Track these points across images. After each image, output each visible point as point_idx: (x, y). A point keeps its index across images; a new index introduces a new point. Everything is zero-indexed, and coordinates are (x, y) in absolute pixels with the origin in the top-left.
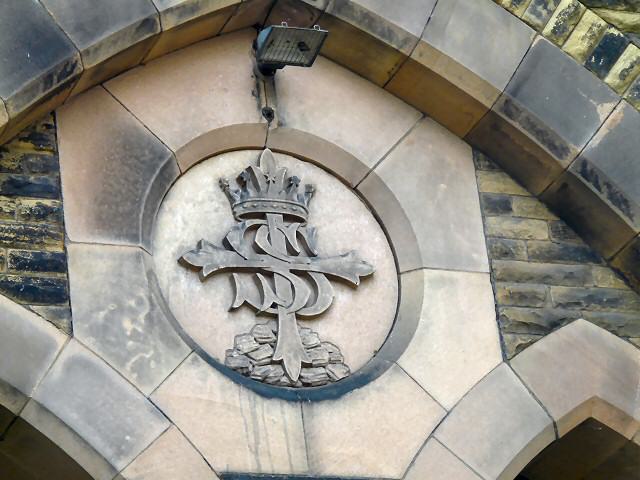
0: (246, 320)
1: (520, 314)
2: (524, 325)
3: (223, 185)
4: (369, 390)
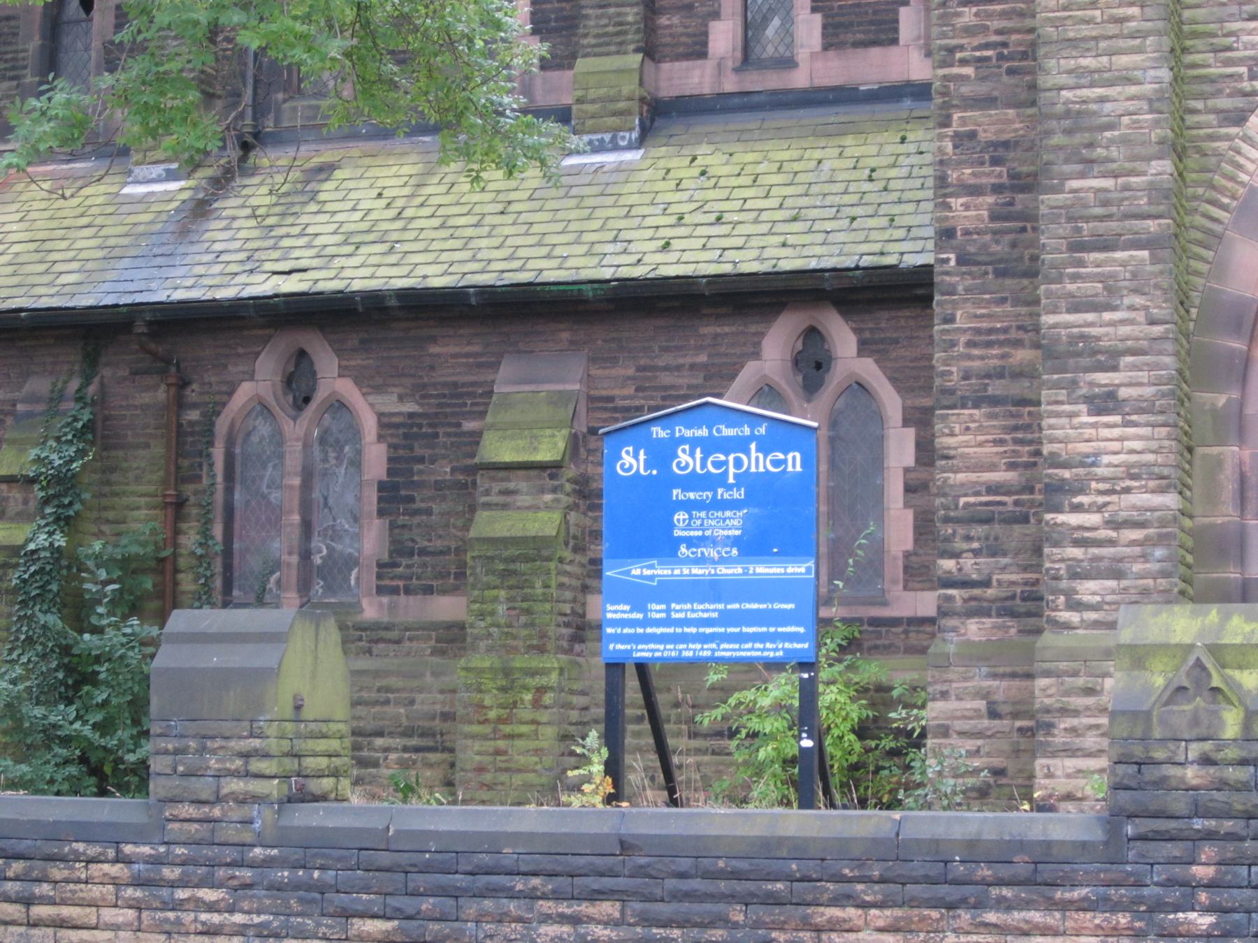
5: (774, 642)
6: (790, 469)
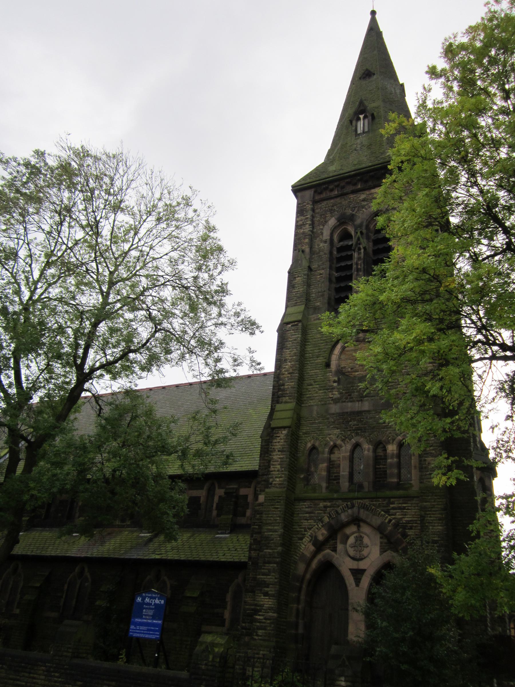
2: (383, 551)
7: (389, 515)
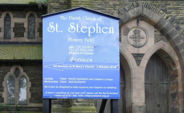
0: (134, 42)
1: (156, 40)
2: (157, 41)
3: (133, 31)
4: (143, 47)
5: (106, 92)
6: (110, 32)
7: (167, 13)
